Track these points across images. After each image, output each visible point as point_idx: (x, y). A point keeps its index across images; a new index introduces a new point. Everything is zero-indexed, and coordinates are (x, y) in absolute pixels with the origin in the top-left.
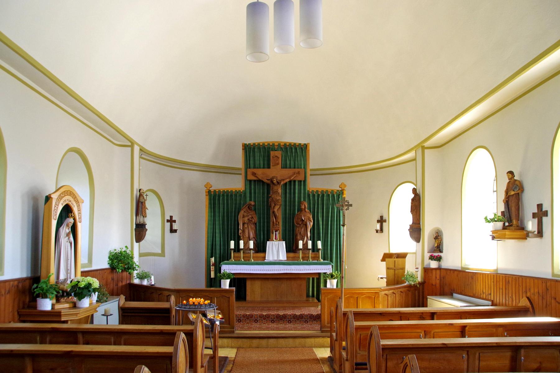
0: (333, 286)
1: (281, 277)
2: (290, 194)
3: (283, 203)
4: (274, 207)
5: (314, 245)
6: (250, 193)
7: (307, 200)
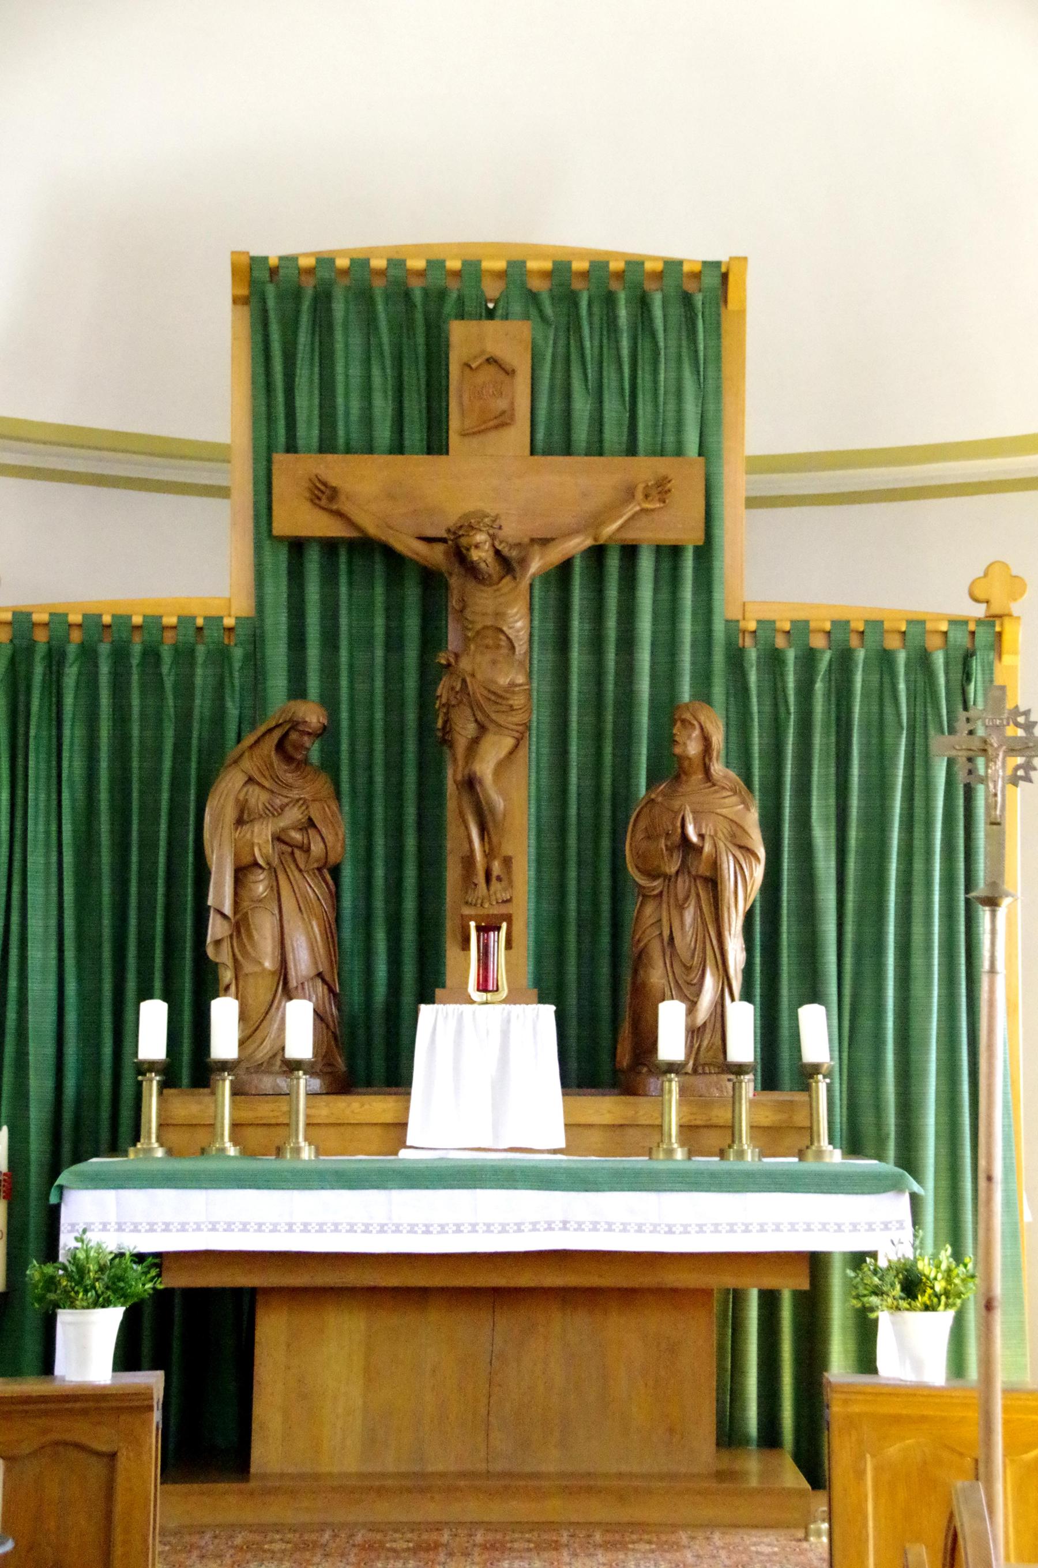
0: (918, 1366)
1: (525, 1279)
2: (596, 644)
3: (541, 718)
4: (475, 741)
5: (773, 1033)
7: (718, 691)
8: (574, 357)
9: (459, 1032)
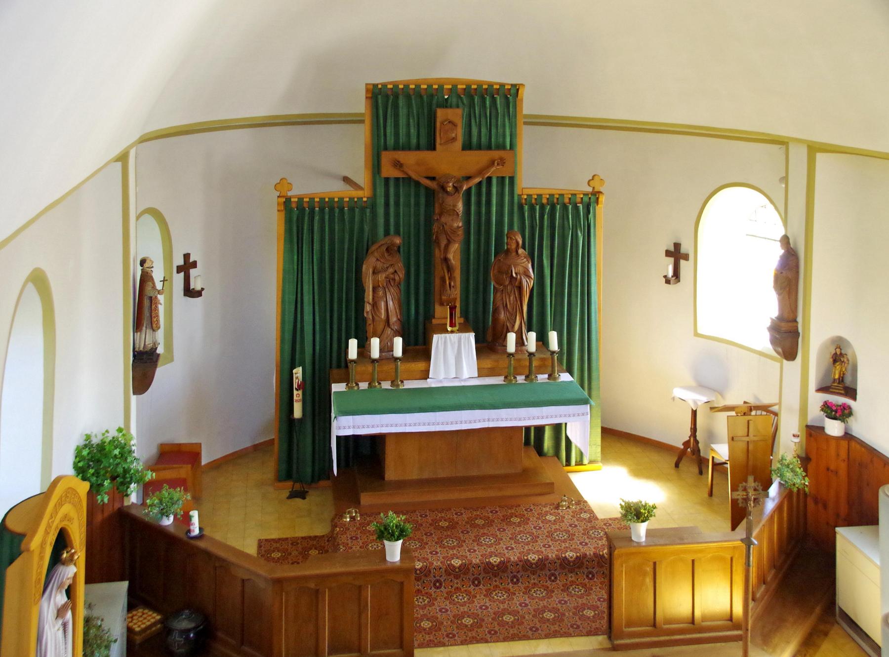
2: (479, 203)
6: (387, 205)
8: (472, 115)
9: (445, 342)
